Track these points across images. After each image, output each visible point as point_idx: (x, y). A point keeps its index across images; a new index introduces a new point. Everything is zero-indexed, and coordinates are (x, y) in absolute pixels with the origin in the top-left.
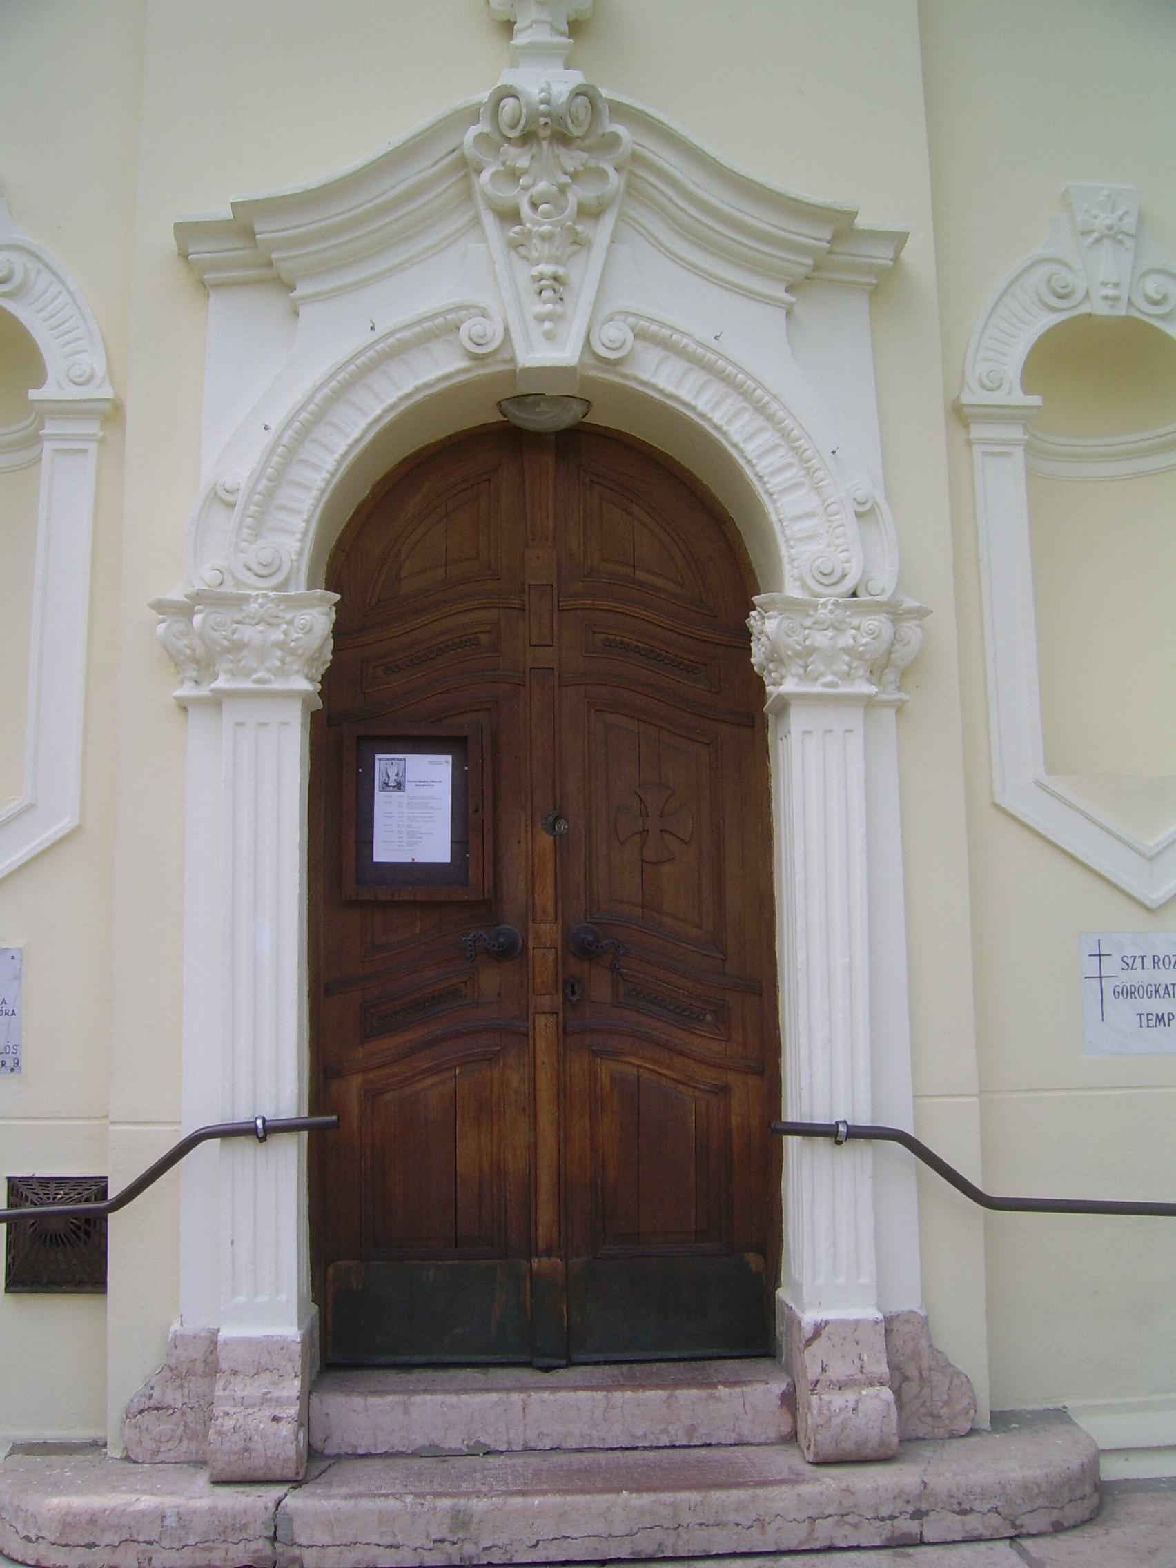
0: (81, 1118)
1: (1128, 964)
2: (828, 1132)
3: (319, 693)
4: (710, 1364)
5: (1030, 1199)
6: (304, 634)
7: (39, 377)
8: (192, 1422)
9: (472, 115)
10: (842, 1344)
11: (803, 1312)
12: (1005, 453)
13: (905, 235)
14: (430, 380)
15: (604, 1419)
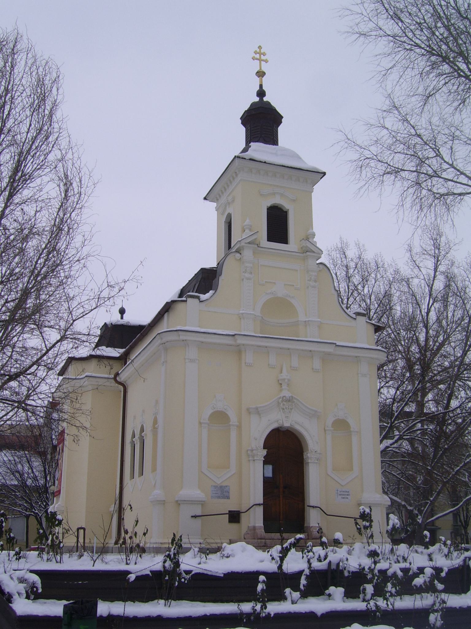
1: (340, 492)
3: (282, 117)
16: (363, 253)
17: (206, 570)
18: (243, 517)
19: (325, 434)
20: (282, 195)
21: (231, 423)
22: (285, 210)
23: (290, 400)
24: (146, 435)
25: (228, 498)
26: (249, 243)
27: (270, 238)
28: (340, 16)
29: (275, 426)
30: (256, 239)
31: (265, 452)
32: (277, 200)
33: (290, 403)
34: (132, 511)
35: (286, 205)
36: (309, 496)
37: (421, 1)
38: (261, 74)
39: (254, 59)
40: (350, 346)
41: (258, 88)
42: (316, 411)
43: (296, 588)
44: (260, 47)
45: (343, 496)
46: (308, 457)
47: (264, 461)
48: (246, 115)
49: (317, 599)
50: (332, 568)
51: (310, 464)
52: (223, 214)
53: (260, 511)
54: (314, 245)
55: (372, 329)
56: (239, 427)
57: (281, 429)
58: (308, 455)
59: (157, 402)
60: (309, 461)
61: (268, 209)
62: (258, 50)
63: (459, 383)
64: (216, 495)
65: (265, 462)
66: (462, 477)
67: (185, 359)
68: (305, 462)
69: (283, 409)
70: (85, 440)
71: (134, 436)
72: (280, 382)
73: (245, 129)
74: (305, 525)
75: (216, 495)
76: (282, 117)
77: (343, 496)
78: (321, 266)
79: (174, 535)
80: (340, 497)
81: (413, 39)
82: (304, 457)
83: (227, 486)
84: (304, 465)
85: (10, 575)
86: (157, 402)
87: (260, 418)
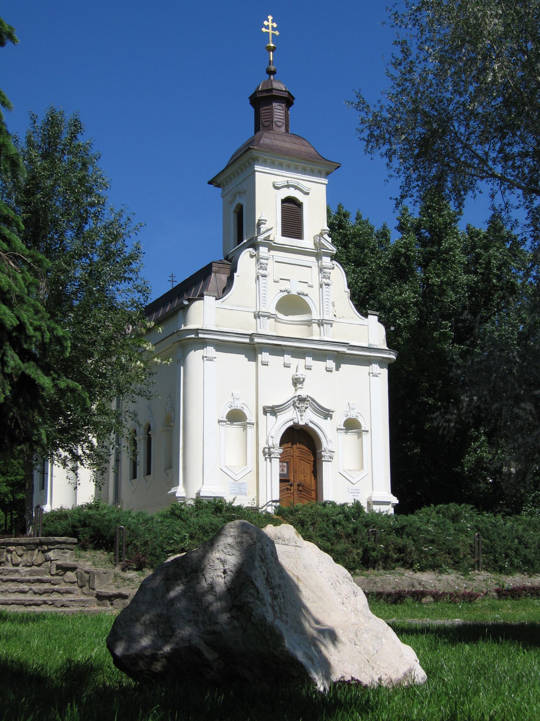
0: (13, 604)
1: (351, 490)
2: (366, 361)
3: (249, 361)
4: (413, 586)
5: (243, 227)
6: (442, 567)
7: (247, 419)
8: (411, 196)
9: (295, 397)
10: (379, 101)
11: (18, 616)
12: (313, 423)
13: (210, 183)
14: (62, 589)
15: (302, 400)
17: (17, 600)
18: (351, 437)
20: (296, 188)
21: (248, 421)
22: (299, 203)
27: (286, 233)
28: (129, 219)
30: (269, 236)
34: (392, 54)
36: (130, 474)
37: (459, 1)
39: (398, 219)
40: (239, 332)
43: (10, 381)
45: (354, 494)
50: (260, 247)
52: (231, 203)
57: (295, 428)
64: (234, 491)
66: (109, 667)
73: (254, 110)
75: (234, 491)
76: (249, 361)
77: (354, 494)
81: (254, 421)
85: (262, 364)
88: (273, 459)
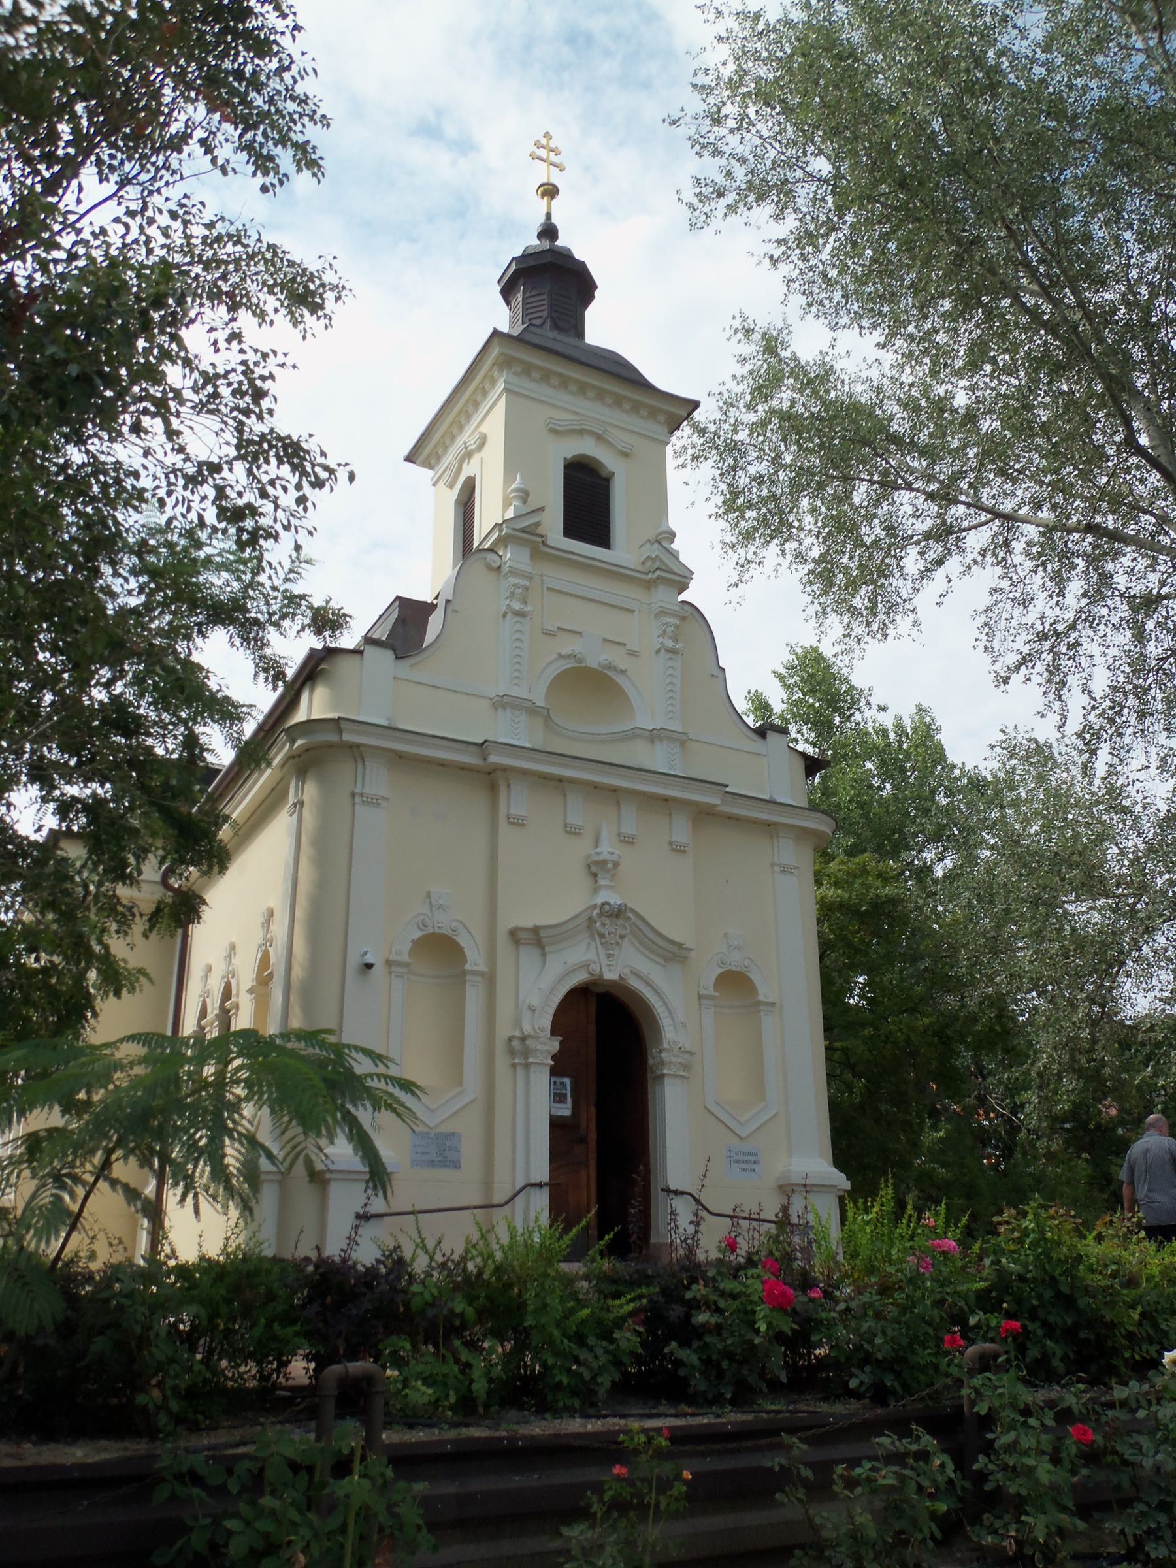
2: (770, 829)
16: (1051, 696)
19: (354, 804)
20: (599, 438)
21: (467, 967)
22: (604, 474)
23: (616, 913)
24: (237, 1007)
25: (456, 1165)
26: (523, 530)
29: (580, 978)
30: (537, 524)
31: (555, 1045)
32: (586, 448)
33: (620, 922)
35: (608, 460)
38: (550, 191)
39: (534, 157)
41: (542, 219)
42: (680, 946)
44: (547, 135)
45: (744, 1166)
46: (662, 1063)
47: (552, 1068)
48: (513, 267)
49: (448, 581)
51: (667, 1081)
53: (541, 1202)
54: (675, 555)
55: (800, 766)
56: (490, 979)
58: (663, 1055)
59: (270, 914)
60: (665, 1071)
61: (566, 467)
62: (544, 141)
63: (854, 1405)
65: (554, 1072)
67: (353, 795)
68: (650, 1076)
69: (602, 936)
70: (269, 771)
71: (203, 1014)
72: (593, 869)
74: (653, 1240)
77: (744, 1166)
78: (686, 607)
79: (623, 672)
80: (736, 1166)
82: (651, 1061)
83: (453, 1134)
84: (650, 1084)
86: (270, 914)
87: (544, 955)
88: (532, 1068)
